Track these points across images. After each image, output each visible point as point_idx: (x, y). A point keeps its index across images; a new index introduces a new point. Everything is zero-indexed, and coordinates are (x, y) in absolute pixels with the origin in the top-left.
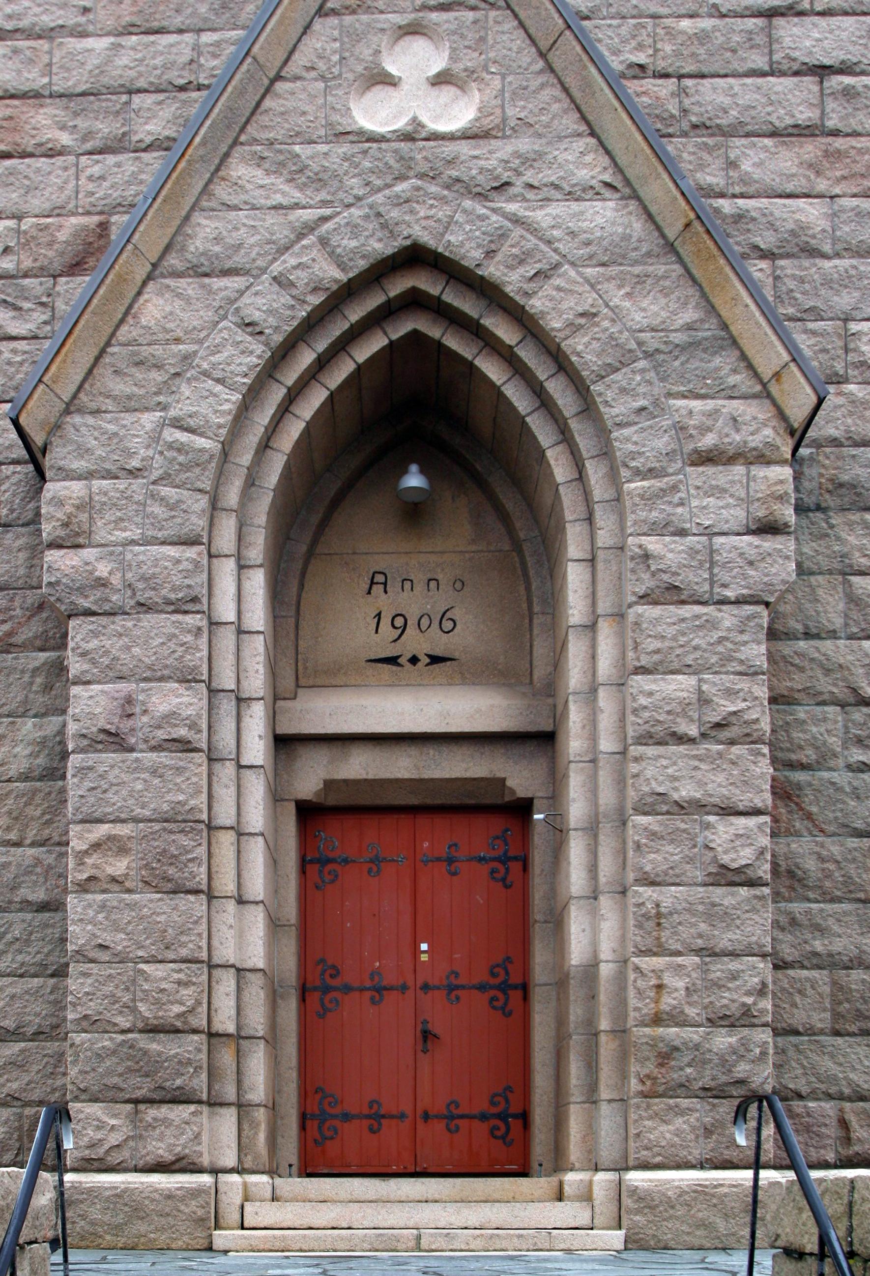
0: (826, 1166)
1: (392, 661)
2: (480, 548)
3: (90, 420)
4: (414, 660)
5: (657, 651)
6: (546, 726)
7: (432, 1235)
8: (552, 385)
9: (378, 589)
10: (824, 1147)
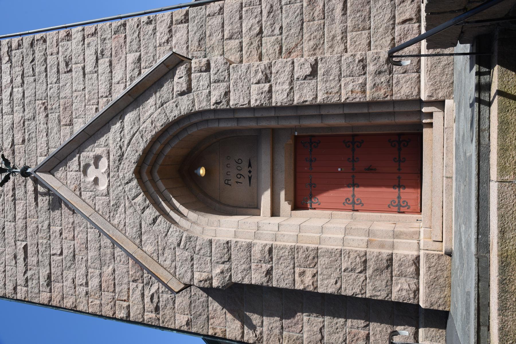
0: (420, 26)
1: (250, 178)
3: (178, 270)
4: (250, 172)
5: (244, 98)
7: (446, 172)
9: (230, 182)
10: (413, 28)
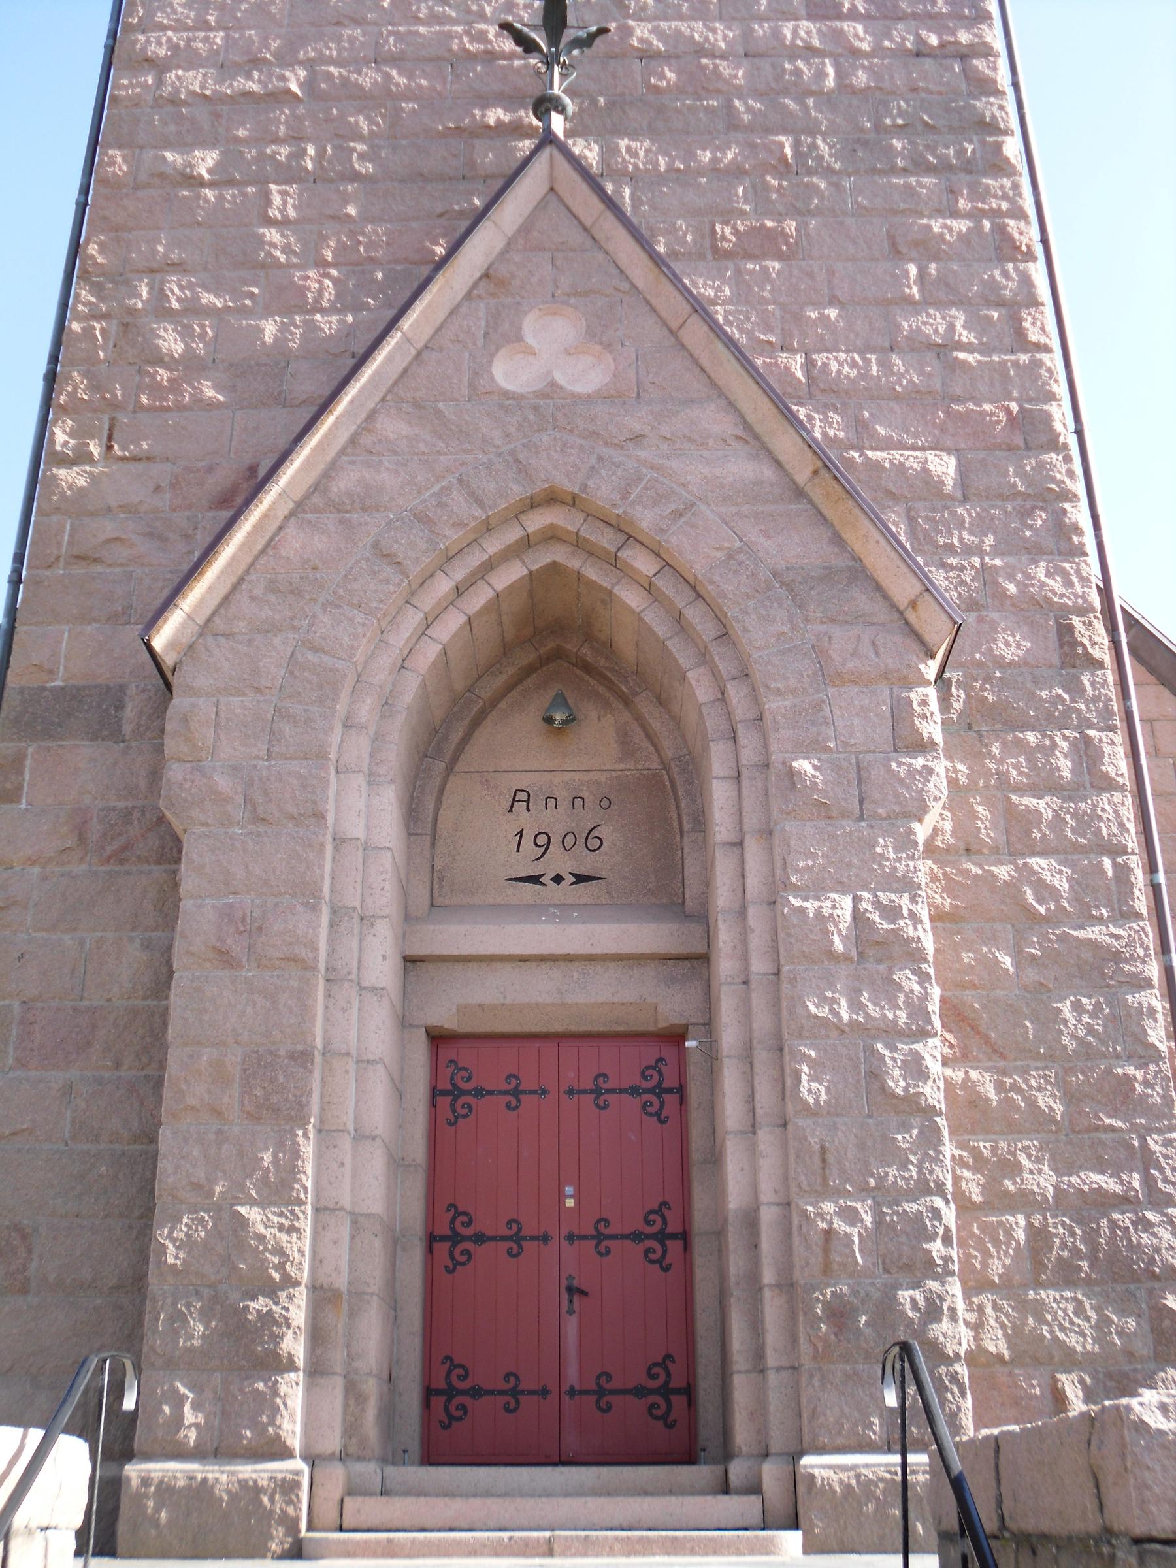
1: (535, 879)
2: (628, 767)
4: (558, 879)
6: (698, 948)
8: (691, 612)
